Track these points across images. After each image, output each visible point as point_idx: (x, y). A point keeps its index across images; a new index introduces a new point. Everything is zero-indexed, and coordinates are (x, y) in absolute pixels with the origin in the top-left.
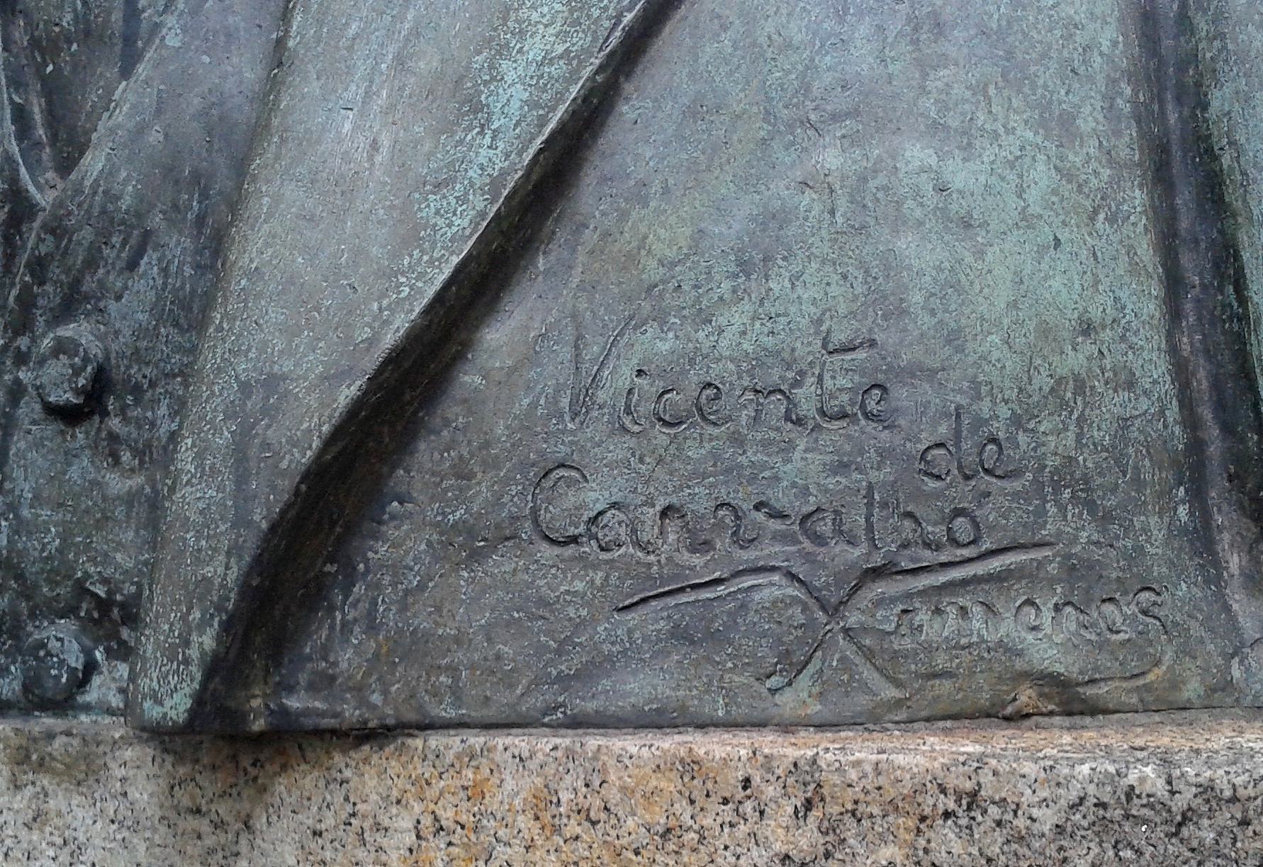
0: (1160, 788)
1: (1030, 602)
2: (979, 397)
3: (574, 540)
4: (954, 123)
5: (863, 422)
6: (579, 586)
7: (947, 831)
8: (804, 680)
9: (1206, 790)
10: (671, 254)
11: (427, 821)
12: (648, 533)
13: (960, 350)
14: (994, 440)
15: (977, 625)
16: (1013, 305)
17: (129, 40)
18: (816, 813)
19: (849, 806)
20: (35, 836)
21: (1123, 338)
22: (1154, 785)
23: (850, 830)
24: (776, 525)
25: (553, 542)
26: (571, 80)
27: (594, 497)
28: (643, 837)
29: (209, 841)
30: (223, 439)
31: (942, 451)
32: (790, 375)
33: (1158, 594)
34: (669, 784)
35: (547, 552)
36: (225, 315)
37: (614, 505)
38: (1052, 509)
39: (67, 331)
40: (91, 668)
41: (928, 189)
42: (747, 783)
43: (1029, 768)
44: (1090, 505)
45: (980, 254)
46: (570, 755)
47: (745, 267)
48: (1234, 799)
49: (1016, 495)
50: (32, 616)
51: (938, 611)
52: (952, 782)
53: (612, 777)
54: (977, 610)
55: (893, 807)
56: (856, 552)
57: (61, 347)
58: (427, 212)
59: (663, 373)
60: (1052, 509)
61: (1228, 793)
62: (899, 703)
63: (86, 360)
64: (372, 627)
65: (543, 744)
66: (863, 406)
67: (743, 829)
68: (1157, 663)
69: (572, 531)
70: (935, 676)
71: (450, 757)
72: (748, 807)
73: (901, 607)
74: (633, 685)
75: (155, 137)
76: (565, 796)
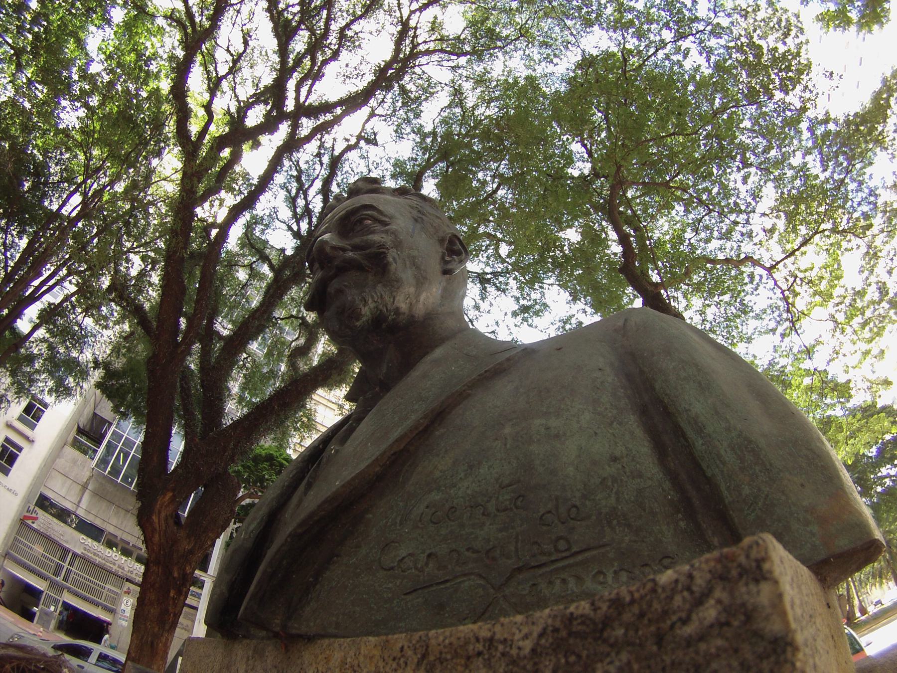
1: (600, 572)
3: (392, 568)
5: (515, 510)
6: (390, 585)
14: (575, 506)
19: (438, 656)
21: (633, 460)
22: (584, 608)
25: (385, 570)
31: (550, 515)
32: (485, 499)
33: (673, 559)
37: (410, 555)
48: (633, 601)
51: (550, 583)
61: (628, 599)
66: (515, 505)
69: (392, 565)
73: (531, 583)
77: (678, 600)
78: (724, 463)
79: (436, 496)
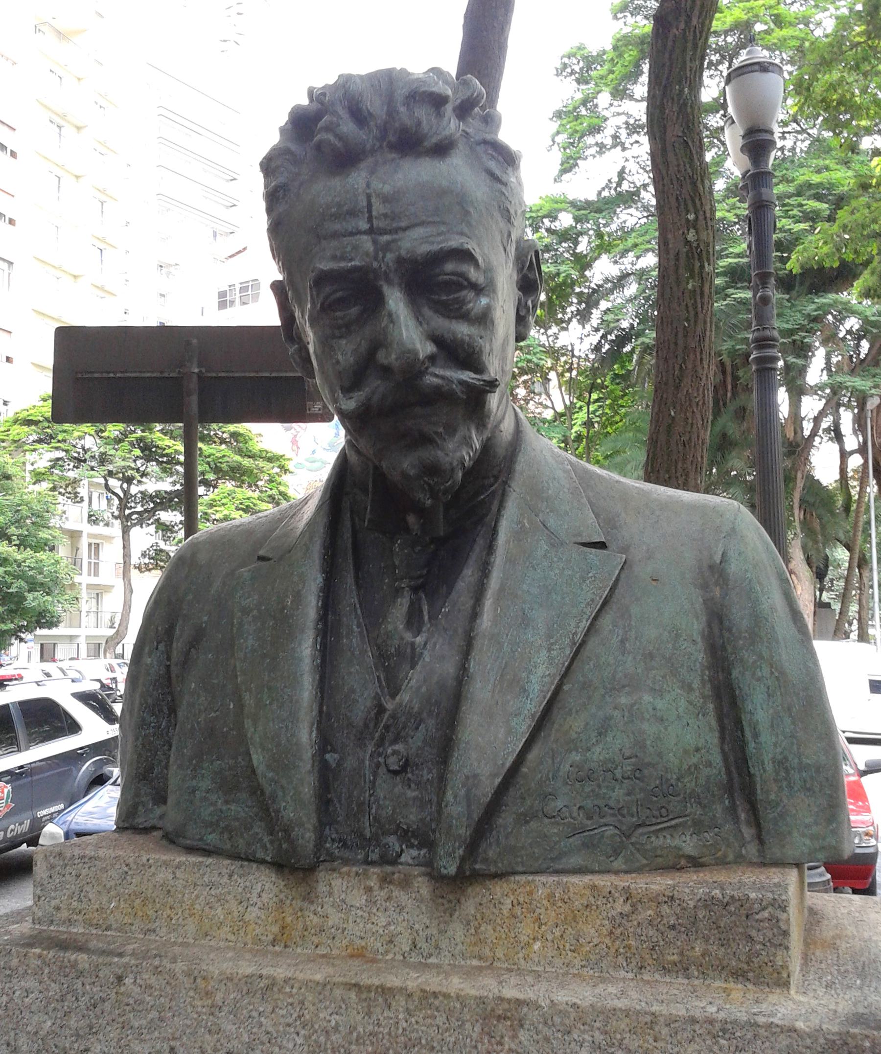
0: (720, 896)
1: (683, 834)
2: (667, 772)
3: (554, 817)
4: (657, 688)
6: (556, 831)
7: (665, 907)
8: (620, 859)
9: (732, 897)
10: (579, 730)
11: (515, 902)
12: (575, 814)
13: (661, 758)
15: (669, 841)
16: (676, 744)
17: (413, 658)
18: (629, 901)
20: (388, 904)
23: (639, 906)
24: (611, 811)
26: (552, 683)
27: (559, 804)
28: (580, 907)
29: (446, 906)
30: (463, 792)
34: (588, 892)
35: (547, 821)
36: (459, 755)
38: (688, 805)
39: (396, 747)
40: (402, 851)
41: (650, 709)
42: (610, 892)
43: (687, 890)
44: (700, 803)
45: (666, 729)
46: (558, 883)
47: (600, 734)
49: (678, 802)
50: (383, 834)
52: (666, 893)
53: (571, 890)
54: (668, 836)
55: (651, 900)
56: (634, 819)
57: (394, 753)
58: (513, 724)
59: (577, 766)
60: (688, 805)
62: (647, 865)
63: (402, 757)
64: (498, 843)
65: (552, 879)
67: (609, 905)
68: (720, 850)
70: (656, 856)
71: (522, 882)
72: (610, 899)
74: (572, 861)
75: (424, 689)
76: (557, 895)
77: (756, 906)
78: (765, 771)
79: (576, 757)
